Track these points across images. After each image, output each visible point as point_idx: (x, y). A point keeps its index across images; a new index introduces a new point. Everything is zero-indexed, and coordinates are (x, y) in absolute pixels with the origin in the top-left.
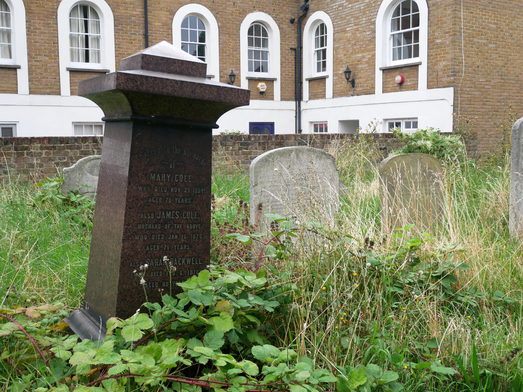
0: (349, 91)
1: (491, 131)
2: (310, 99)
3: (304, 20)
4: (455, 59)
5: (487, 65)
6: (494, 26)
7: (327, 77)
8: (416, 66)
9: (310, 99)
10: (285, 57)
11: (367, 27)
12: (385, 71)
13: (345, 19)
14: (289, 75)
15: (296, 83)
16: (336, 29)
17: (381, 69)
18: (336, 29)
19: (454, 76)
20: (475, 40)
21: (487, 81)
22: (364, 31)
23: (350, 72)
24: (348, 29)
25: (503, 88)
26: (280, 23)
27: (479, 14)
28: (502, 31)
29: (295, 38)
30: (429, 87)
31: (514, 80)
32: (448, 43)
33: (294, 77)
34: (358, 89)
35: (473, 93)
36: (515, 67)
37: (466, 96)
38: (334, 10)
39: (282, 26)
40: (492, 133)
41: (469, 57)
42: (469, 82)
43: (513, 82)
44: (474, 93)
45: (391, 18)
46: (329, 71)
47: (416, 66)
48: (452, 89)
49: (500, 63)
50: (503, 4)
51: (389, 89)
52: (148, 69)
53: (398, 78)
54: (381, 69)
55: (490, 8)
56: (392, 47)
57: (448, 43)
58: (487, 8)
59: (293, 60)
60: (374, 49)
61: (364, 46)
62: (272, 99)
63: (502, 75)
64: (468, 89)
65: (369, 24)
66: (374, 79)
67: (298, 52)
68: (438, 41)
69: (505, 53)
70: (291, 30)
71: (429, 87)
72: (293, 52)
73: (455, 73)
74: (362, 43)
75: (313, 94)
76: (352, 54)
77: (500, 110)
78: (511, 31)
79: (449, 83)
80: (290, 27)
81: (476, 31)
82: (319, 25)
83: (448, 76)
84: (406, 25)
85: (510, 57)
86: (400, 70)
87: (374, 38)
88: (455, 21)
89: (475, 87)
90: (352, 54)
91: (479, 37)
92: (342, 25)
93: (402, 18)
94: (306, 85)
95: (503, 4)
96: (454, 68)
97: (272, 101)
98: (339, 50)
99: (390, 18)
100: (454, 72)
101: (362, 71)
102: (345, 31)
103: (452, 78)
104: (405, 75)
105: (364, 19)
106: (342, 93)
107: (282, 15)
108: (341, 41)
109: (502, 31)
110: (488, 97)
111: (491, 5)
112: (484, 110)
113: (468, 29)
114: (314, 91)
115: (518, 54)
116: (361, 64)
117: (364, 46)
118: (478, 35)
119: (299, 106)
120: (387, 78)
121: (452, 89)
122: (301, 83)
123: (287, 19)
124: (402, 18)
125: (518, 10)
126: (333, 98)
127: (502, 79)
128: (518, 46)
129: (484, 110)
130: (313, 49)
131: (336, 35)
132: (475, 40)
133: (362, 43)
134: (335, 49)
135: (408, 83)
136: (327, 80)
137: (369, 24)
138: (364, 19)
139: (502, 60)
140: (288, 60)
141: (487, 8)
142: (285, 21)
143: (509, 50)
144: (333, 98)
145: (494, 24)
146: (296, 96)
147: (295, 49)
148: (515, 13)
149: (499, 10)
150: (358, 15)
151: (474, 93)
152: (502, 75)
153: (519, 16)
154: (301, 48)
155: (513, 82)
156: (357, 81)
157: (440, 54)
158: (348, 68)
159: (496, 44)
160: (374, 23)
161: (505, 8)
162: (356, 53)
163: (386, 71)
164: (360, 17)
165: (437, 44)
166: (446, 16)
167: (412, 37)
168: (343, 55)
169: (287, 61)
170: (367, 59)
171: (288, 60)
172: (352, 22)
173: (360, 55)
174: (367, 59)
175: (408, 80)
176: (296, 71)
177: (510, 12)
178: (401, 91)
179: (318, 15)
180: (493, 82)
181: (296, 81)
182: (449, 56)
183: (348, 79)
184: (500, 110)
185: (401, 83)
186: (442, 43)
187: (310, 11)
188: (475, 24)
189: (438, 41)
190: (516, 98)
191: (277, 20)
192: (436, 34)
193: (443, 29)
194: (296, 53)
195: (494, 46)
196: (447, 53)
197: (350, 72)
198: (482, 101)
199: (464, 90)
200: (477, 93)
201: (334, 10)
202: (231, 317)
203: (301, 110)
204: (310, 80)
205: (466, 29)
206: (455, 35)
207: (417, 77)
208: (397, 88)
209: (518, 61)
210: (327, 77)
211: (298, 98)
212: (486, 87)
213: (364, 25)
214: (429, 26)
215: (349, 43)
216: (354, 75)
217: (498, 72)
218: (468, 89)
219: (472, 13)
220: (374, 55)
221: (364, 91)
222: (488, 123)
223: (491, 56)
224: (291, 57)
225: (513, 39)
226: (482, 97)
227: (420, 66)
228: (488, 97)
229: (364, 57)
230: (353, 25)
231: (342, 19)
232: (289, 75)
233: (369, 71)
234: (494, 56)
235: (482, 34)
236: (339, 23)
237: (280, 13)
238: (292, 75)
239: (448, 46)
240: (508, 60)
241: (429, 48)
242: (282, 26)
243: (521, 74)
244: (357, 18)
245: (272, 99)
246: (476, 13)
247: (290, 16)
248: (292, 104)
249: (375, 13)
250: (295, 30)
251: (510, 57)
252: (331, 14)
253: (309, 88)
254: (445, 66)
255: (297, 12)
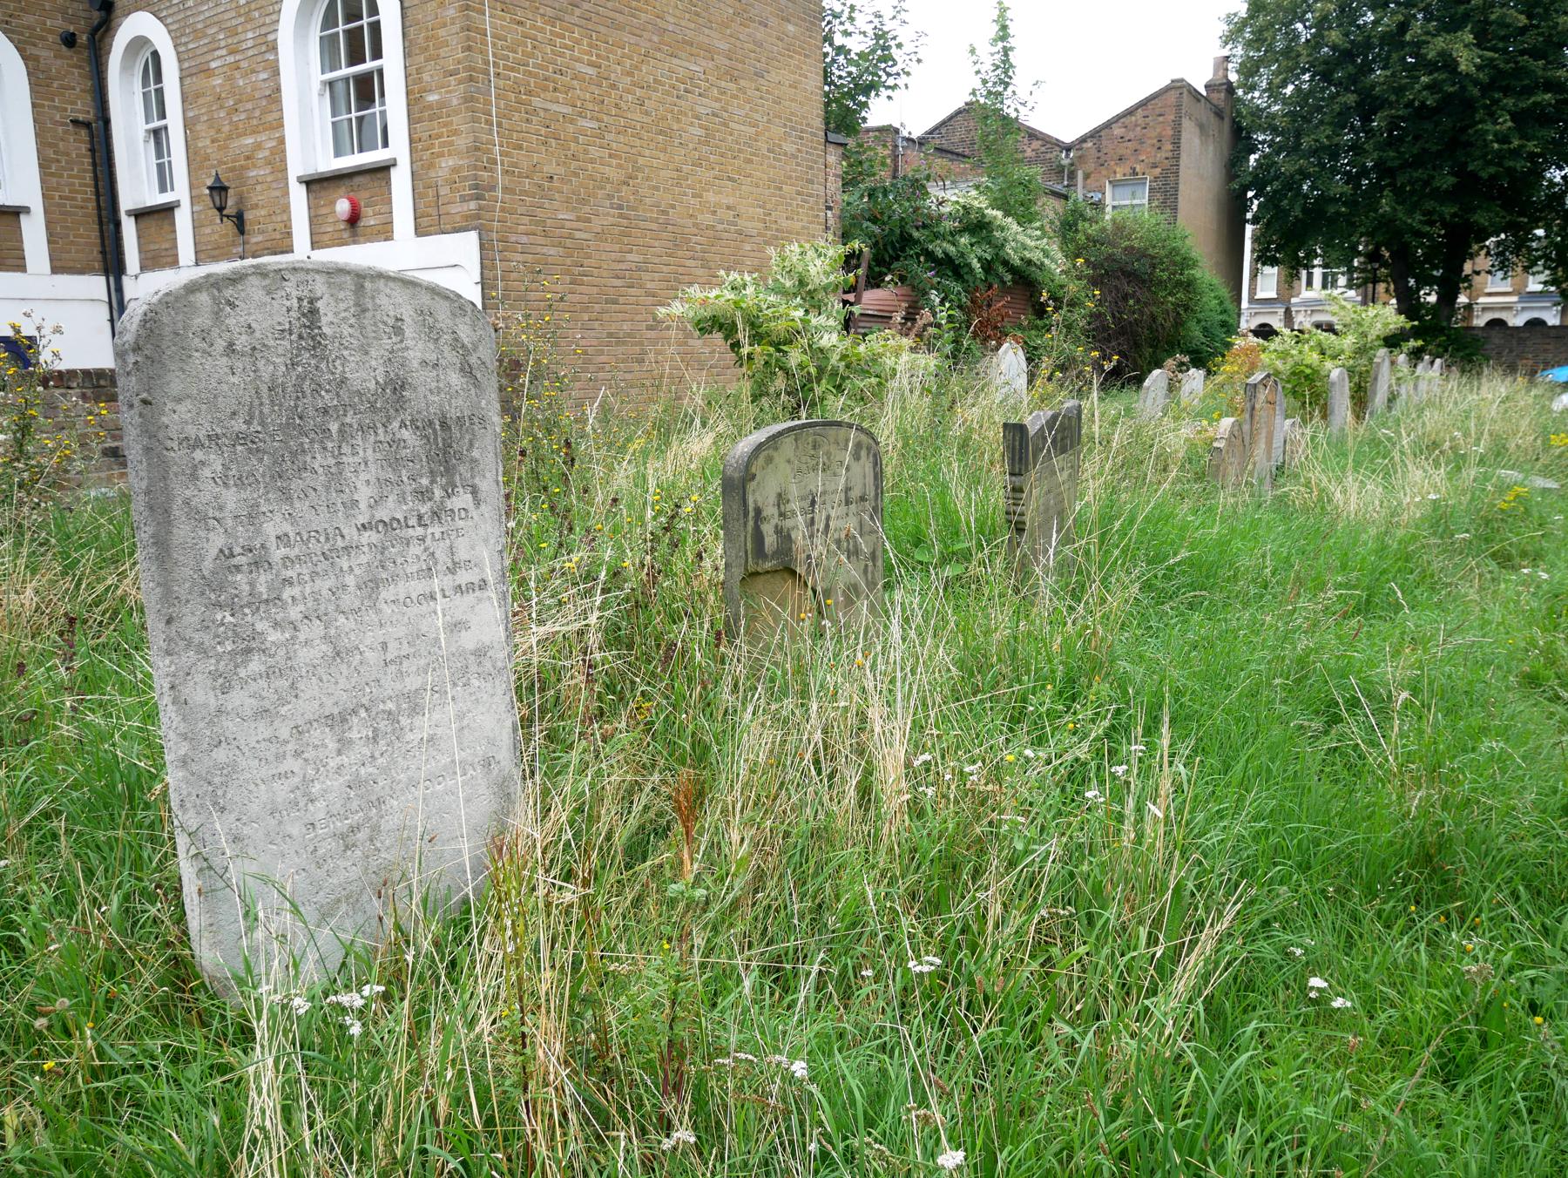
0: (234, 244)
1: (601, 353)
2: (143, 268)
3: (107, 40)
4: (477, 149)
5: (576, 175)
6: (591, 71)
7: (177, 204)
8: (382, 171)
9: (143, 268)
10: (56, 145)
11: (259, 59)
12: (314, 187)
13: (206, 36)
14: (74, 199)
15: (101, 223)
16: (186, 65)
17: (301, 180)
18: (186, 65)
19: (478, 198)
20: (536, 102)
21: (579, 219)
22: (253, 71)
23: (225, 189)
24: (213, 65)
25: (626, 240)
26: (26, 42)
27: (542, 30)
28: (613, 86)
29: (82, 91)
30: (420, 231)
31: (655, 220)
32: (455, 102)
33: (92, 205)
34: (254, 240)
35: (539, 249)
36: (657, 188)
37: (520, 257)
38: (175, 9)
39: (30, 50)
40: (604, 358)
41: (521, 148)
42: (526, 219)
43: (654, 226)
44: (545, 250)
45: (318, 34)
46: (180, 191)
47: (382, 171)
48: (473, 236)
49: (612, 173)
50: (611, 14)
51: (326, 238)
52: (216, 259)
53: (343, 207)
54: (301, 180)
55: (576, 20)
56: (330, 119)
57: (455, 102)
58: (567, 18)
59: (84, 156)
60: (279, 124)
61: (257, 113)
62: (21, 267)
63: (620, 207)
64: (524, 239)
65: (264, 48)
66: (286, 209)
67: (98, 132)
68: (432, 98)
69: (627, 149)
70: (69, 69)
71: (420, 231)
72: (84, 132)
73: (480, 191)
74: (249, 106)
75: (149, 255)
76: (229, 138)
77: (621, 300)
78: (638, 92)
79: (467, 218)
80: (62, 57)
81: (536, 76)
82: (148, 54)
83: (464, 199)
84: (356, 57)
85: (641, 161)
86: (347, 182)
87: (278, 90)
88: (468, 39)
89: (545, 234)
90: (229, 138)
91: (549, 95)
92: (199, 52)
93: (347, 32)
94: (129, 228)
95: (611, 14)
96: (476, 177)
97: (18, 275)
98: (198, 127)
99: (315, 33)
100: (476, 187)
101: (258, 188)
102: (207, 72)
103: (473, 205)
104: (362, 197)
105: (250, 35)
106: (216, 252)
107: (29, 19)
108: (201, 101)
109: (613, 86)
110: (586, 262)
111: (577, 12)
112: (577, 298)
113: (512, 69)
114: (152, 247)
115: (661, 155)
116: (255, 166)
117: (257, 113)
118: (545, 89)
119: (119, 290)
120: (318, 207)
121: (473, 236)
122: (118, 224)
123: (50, 31)
124: (347, 32)
125: (655, 39)
126: (197, 264)
127: (621, 216)
128: (661, 133)
129: (577, 298)
130: (141, 127)
131: (188, 81)
132: (536, 102)
133: (249, 106)
134: (188, 124)
135: (369, 220)
136: (177, 213)
137: (264, 48)
138: (250, 35)
139: (620, 166)
140: (68, 154)
141: (567, 18)
142: (43, 38)
143: (638, 142)
144: (197, 264)
145: (591, 64)
146: (105, 260)
147: (87, 125)
148: (648, 45)
149: (602, 29)
150: (234, 22)
151: (545, 250)
152: (620, 207)
153: (658, 55)
154: (107, 122)
155: (654, 226)
156: (248, 216)
157: (439, 136)
158: (217, 178)
159: (598, 120)
160: (273, 48)
161: (620, 27)
162: (239, 136)
163: (316, 184)
164: (240, 29)
165: (430, 107)
166: (445, 25)
167: (367, 90)
168: (208, 142)
169: (63, 159)
170: (267, 153)
171: (68, 154)
172: (223, 44)
173: (249, 141)
174: (267, 153)
175: (370, 211)
176: (96, 186)
177: (633, 39)
178: (355, 242)
179: (136, 25)
180: (596, 225)
181: (100, 217)
182: (462, 142)
183: (220, 209)
184: (621, 300)
185: (353, 219)
186: (442, 105)
187: (118, 12)
188: (531, 56)
189: (432, 98)
190: (665, 269)
191: (13, 32)
192: (426, 77)
193: (441, 62)
194: (92, 136)
195: (595, 125)
196: (456, 133)
197: (225, 189)
198: (568, 272)
199: (513, 239)
200: (553, 251)
201: (175, 9)
202: (501, 687)
203: (126, 298)
204: (140, 215)
205: (506, 67)
206: (471, 79)
207: (390, 202)
208: (346, 235)
209: (662, 173)
210: (177, 204)
211: (113, 266)
212: (578, 234)
213: (251, 53)
214: (407, 54)
215: (222, 107)
216: (241, 199)
217: (610, 197)
218: (524, 239)
219: (520, 23)
220: (282, 141)
221: (269, 244)
222: (592, 333)
223: (586, 152)
224: (77, 146)
225: (647, 113)
226: (568, 261)
227: (393, 171)
228: (586, 262)
229: (258, 146)
230: (224, 52)
231: (198, 34)
232: (74, 199)
233: (274, 185)
234: (594, 152)
235: (555, 90)
236: (191, 46)
237: (22, 10)
238: (84, 200)
239: (457, 113)
240: (639, 169)
241: (412, 120)
242: (30, 50)
243: (673, 207)
244: (233, 32)
245: (21, 267)
246: (533, 27)
247: (59, 24)
248: (96, 285)
249: (274, 17)
250: (80, 67)
251: (641, 161)
252: (169, 20)
253: (139, 237)
254: (455, 170)
255: (83, 14)
